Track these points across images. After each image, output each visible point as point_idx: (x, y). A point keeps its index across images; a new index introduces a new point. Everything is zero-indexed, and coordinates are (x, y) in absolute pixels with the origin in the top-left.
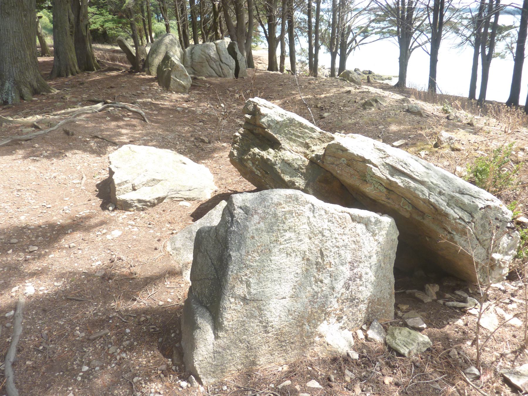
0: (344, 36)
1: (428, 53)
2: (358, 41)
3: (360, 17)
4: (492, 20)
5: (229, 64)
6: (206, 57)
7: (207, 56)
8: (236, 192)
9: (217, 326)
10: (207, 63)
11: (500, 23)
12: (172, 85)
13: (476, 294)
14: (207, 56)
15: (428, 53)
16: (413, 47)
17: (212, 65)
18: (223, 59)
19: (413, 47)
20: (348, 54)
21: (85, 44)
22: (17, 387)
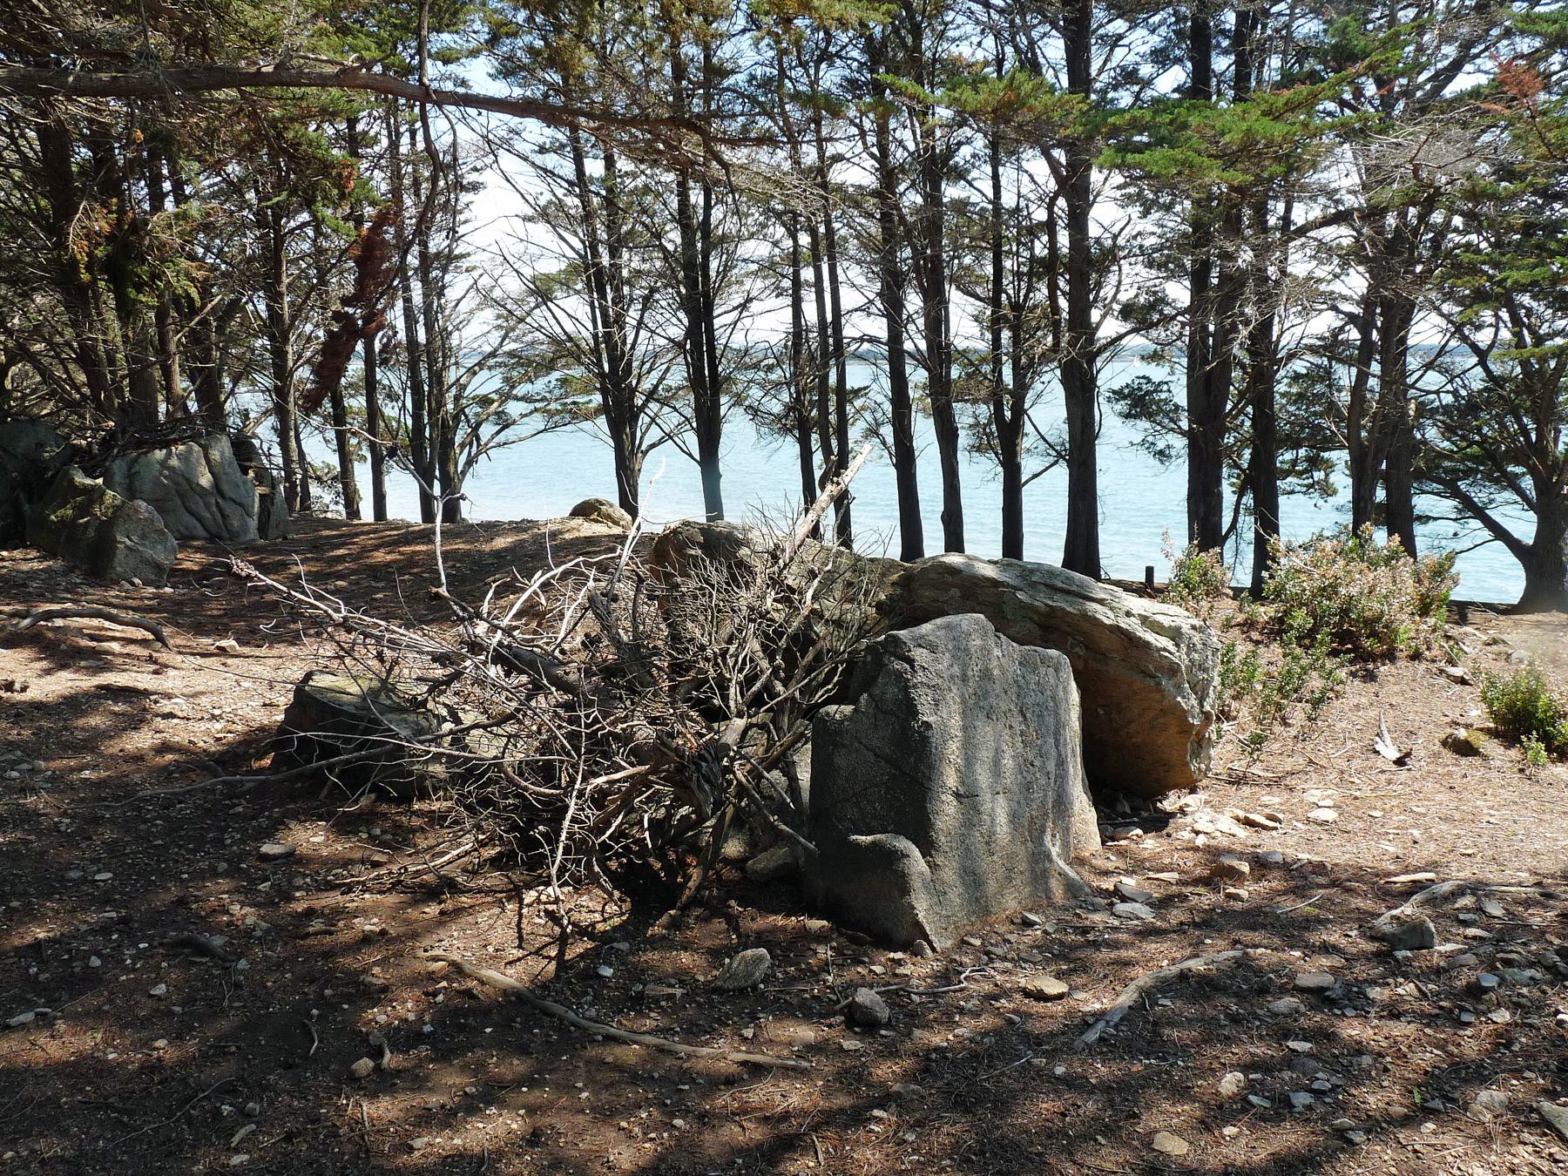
0: (446, 432)
1: (690, 455)
2: (484, 440)
3: (484, 374)
4: (833, 379)
5: (244, 501)
6: (177, 484)
7: (180, 479)
8: (1508, 610)
9: (927, 847)
10: (178, 501)
11: (851, 383)
12: (120, 563)
13: (1533, 695)
14: (180, 479)
15: (690, 455)
16: (644, 448)
17: (193, 507)
18: (225, 488)
19: (644, 448)
20: (464, 473)
21: (900, 286)
22: (1254, 929)
